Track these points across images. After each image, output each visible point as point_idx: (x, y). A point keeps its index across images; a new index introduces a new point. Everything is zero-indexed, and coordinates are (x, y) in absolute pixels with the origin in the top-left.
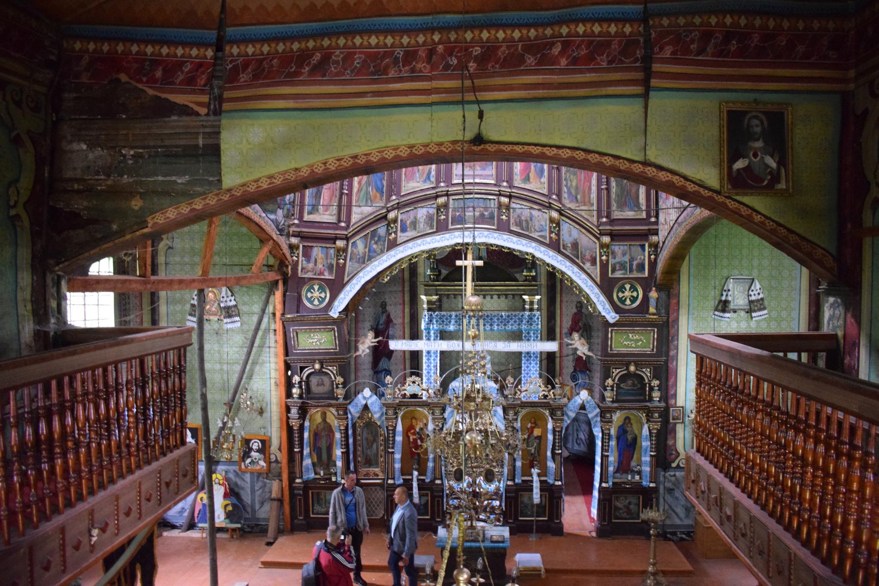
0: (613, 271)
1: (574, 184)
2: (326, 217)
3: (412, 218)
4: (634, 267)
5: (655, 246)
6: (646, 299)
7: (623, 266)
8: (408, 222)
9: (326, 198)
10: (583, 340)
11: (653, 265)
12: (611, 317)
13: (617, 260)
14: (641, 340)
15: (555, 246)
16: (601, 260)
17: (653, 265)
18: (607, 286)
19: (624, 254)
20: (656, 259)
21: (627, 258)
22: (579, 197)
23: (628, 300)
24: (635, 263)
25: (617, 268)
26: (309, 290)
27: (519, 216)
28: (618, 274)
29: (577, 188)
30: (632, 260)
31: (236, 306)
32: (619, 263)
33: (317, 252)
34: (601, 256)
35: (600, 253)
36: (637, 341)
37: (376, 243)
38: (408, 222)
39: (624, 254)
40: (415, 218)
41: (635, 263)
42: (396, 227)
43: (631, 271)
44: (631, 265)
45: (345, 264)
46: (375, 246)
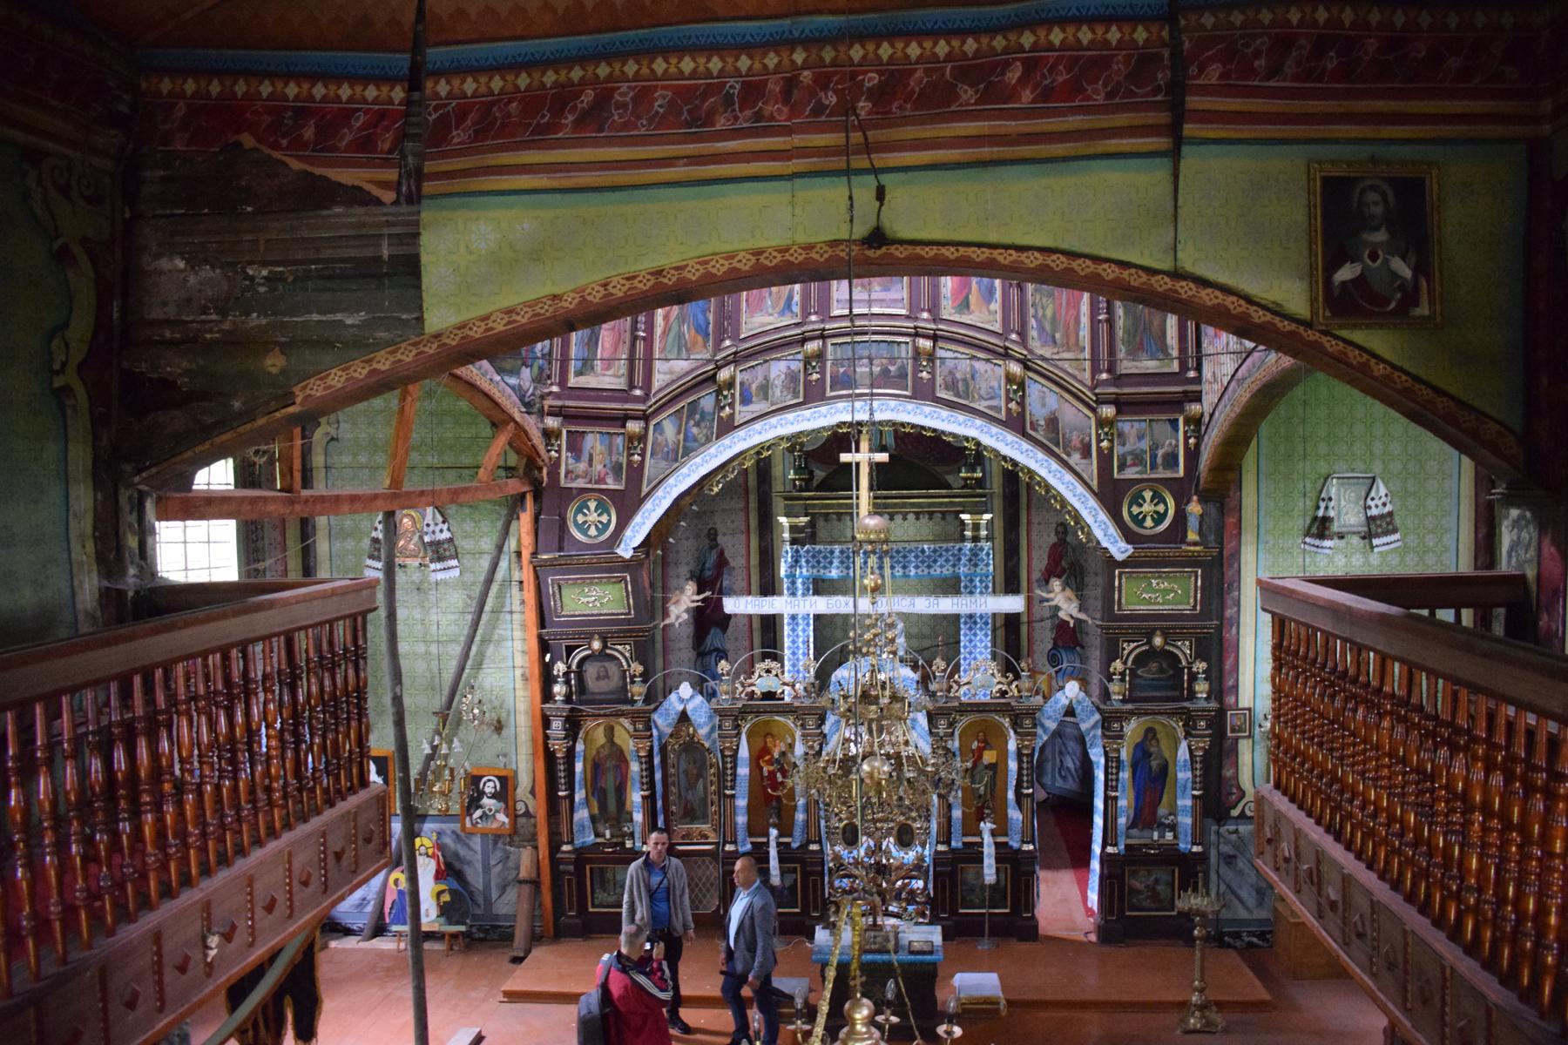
0: (1122, 467)
1: (1049, 313)
2: (607, 379)
3: (760, 378)
4: (1159, 460)
5: (1196, 422)
6: (1181, 517)
7: (1138, 459)
8: (754, 386)
9: (607, 346)
10: (1069, 592)
11: (1193, 456)
12: (1119, 549)
13: (1128, 448)
14: (1172, 590)
15: (1017, 424)
16: (1099, 449)
17: (1193, 456)
18: (1111, 494)
19: (1140, 437)
20: (1197, 445)
21: (1145, 445)
22: (1058, 336)
23: (1149, 519)
24: (1160, 453)
25: (1129, 460)
26: (580, 510)
27: (950, 373)
28: (1131, 473)
29: (1054, 319)
30: (1154, 448)
31: (451, 540)
32: (1132, 453)
33: (593, 441)
34: (1099, 441)
35: (1098, 435)
36: (1166, 591)
37: (697, 424)
38: (754, 386)
39: (1140, 437)
40: (766, 379)
41: (1160, 453)
42: (733, 396)
43: (1154, 467)
44: (1154, 457)
45: (643, 462)
46: (695, 430)
